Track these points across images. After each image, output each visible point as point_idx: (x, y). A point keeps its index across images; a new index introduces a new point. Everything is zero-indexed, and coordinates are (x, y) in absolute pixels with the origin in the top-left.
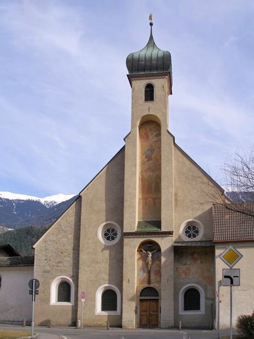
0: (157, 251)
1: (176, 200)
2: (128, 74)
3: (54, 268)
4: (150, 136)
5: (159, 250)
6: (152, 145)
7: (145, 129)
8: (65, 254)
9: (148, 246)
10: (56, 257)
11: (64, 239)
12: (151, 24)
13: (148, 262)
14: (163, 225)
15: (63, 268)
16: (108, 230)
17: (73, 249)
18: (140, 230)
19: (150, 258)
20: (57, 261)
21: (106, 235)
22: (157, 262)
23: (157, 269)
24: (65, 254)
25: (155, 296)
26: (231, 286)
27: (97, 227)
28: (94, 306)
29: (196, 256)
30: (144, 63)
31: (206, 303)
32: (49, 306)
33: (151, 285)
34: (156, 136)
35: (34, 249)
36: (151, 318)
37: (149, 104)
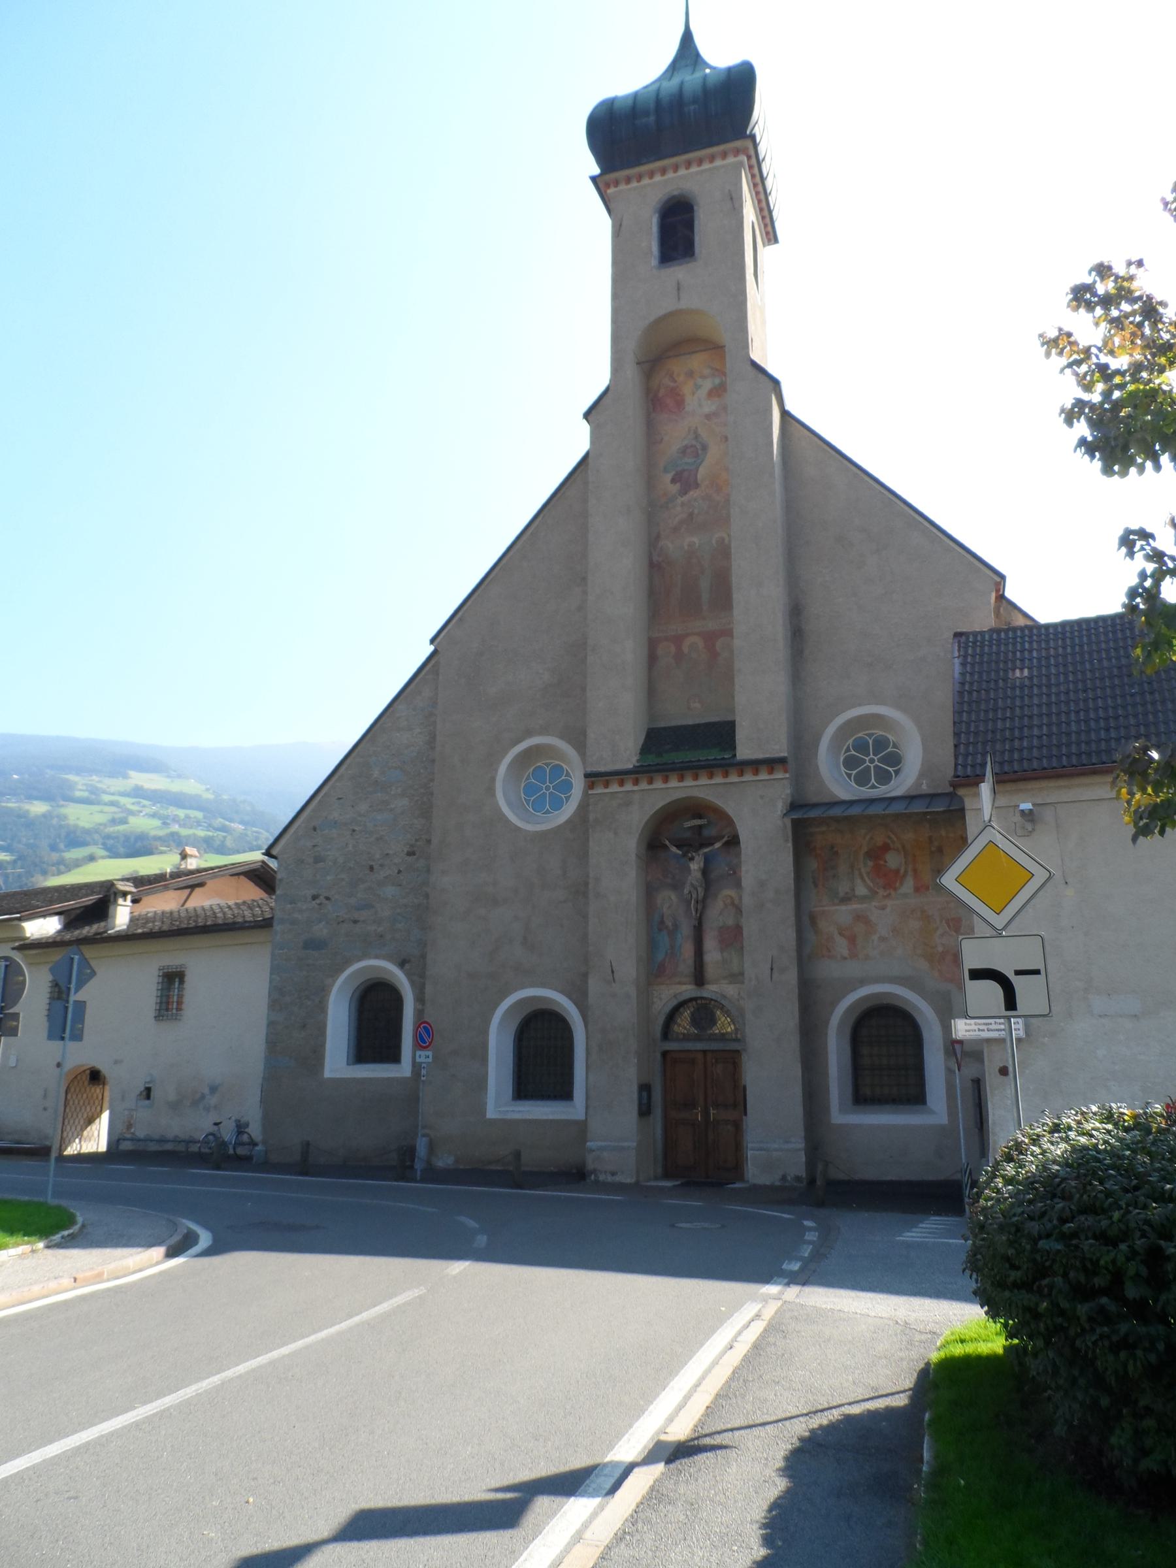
22: (731, 892)
26: (1008, 1018)
30: (652, 118)
37: (679, 272)
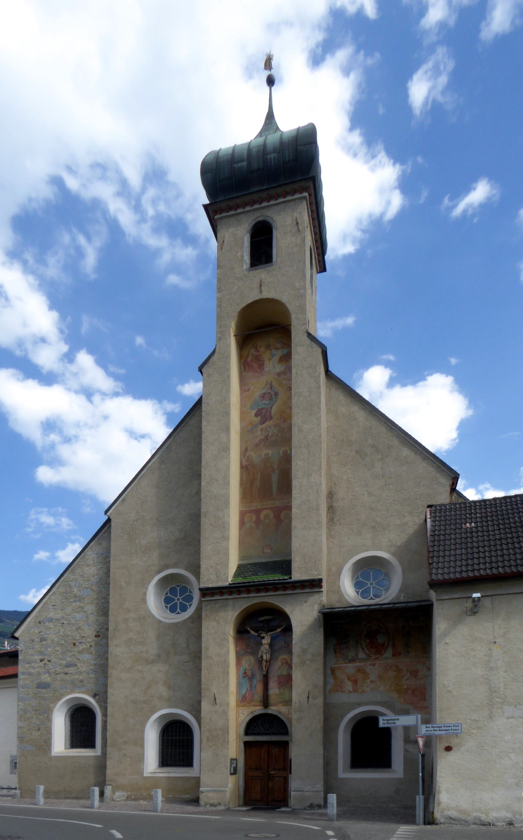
1: (331, 508)
2: (207, 202)
3: (59, 677)
5: (288, 629)
6: (271, 384)
8: (82, 647)
11: (77, 615)
12: (271, 81)
13: (262, 657)
14: (295, 566)
15: (77, 677)
16: (173, 591)
17: (96, 636)
18: (240, 580)
19: (267, 647)
20: (64, 662)
21: (167, 601)
23: (285, 673)
24: (82, 647)
25: (280, 734)
27: (144, 584)
28: (141, 758)
29: (381, 639)
31: (406, 751)
32: (51, 758)
33: (273, 710)
35: (17, 639)
36: (270, 785)
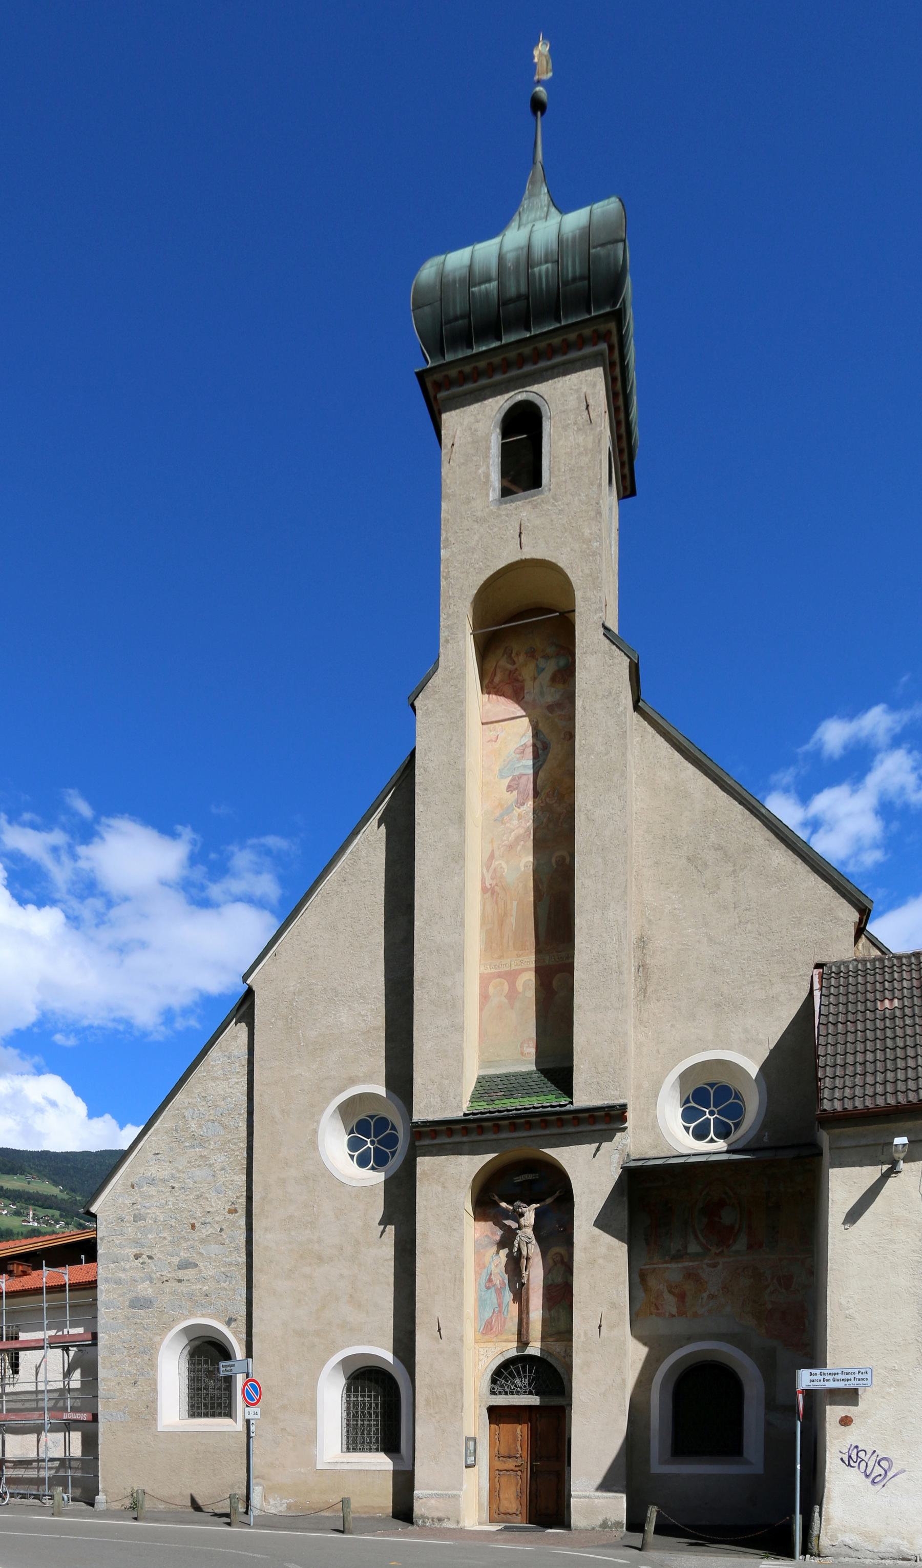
0: (558, 1200)
3: (167, 1287)
4: (528, 684)
7: (509, 654)
8: (205, 1232)
9: (518, 1179)
10: (172, 1242)
11: (197, 1172)
18: (483, 1106)
20: (176, 1260)
24: (205, 1232)
28: (311, 1437)
30: (494, 284)
31: (768, 1424)
34: (554, 679)
